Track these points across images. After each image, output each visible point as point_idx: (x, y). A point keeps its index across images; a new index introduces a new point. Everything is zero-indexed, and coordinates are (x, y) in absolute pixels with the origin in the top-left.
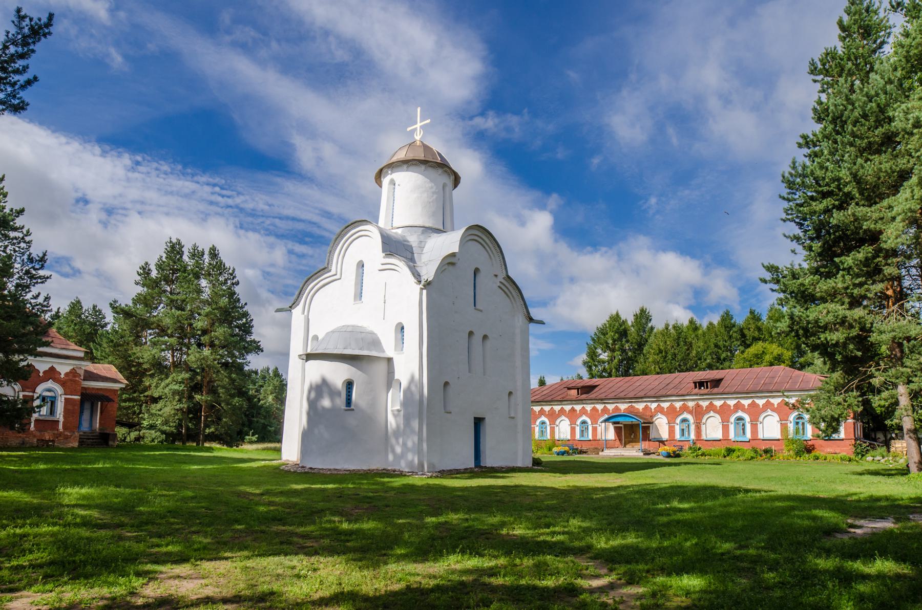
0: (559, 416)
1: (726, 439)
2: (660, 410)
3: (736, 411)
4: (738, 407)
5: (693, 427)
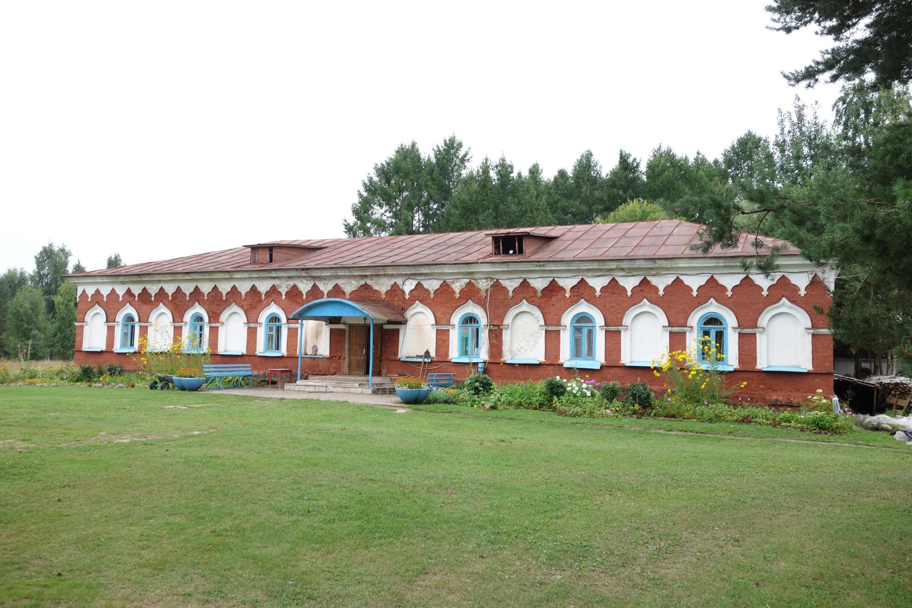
0: (155, 305)
1: (551, 364)
2: (420, 294)
3: (574, 301)
4: (712, 289)
5: (484, 336)
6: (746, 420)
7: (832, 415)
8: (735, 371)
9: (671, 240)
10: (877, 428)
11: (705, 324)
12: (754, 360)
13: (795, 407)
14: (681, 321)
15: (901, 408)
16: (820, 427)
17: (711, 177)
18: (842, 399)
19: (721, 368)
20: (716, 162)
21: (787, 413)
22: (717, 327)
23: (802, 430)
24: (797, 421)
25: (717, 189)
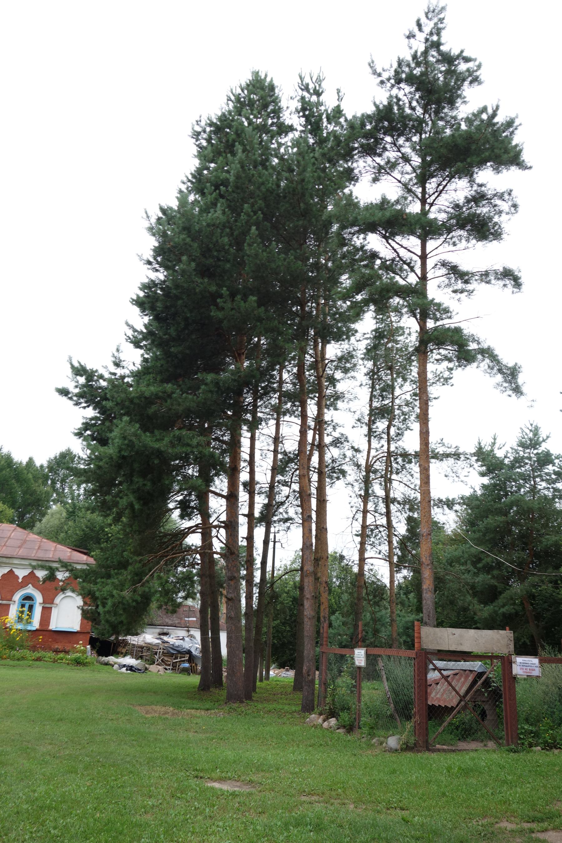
4: (31, 579)
6: (39, 659)
7: (85, 656)
8: (37, 630)
9: (10, 542)
10: (107, 664)
11: (23, 600)
12: (48, 624)
13: (67, 652)
14: (8, 597)
15: (122, 653)
16: (78, 663)
17: (36, 478)
18: (93, 648)
19: (29, 628)
20: (42, 466)
21: (61, 655)
22: (30, 602)
23: (68, 664)
24: (66, 659)
25: (38, 490)
